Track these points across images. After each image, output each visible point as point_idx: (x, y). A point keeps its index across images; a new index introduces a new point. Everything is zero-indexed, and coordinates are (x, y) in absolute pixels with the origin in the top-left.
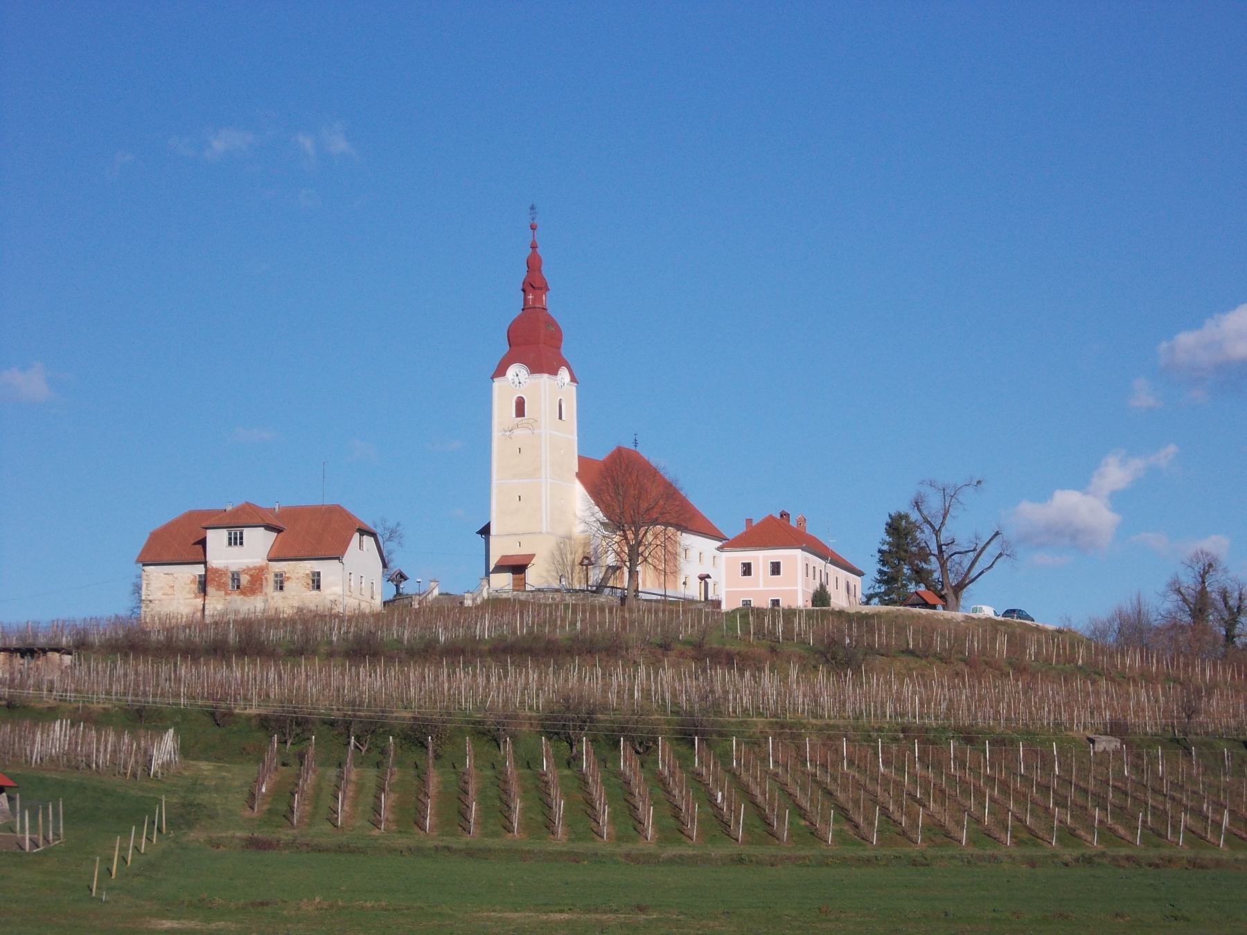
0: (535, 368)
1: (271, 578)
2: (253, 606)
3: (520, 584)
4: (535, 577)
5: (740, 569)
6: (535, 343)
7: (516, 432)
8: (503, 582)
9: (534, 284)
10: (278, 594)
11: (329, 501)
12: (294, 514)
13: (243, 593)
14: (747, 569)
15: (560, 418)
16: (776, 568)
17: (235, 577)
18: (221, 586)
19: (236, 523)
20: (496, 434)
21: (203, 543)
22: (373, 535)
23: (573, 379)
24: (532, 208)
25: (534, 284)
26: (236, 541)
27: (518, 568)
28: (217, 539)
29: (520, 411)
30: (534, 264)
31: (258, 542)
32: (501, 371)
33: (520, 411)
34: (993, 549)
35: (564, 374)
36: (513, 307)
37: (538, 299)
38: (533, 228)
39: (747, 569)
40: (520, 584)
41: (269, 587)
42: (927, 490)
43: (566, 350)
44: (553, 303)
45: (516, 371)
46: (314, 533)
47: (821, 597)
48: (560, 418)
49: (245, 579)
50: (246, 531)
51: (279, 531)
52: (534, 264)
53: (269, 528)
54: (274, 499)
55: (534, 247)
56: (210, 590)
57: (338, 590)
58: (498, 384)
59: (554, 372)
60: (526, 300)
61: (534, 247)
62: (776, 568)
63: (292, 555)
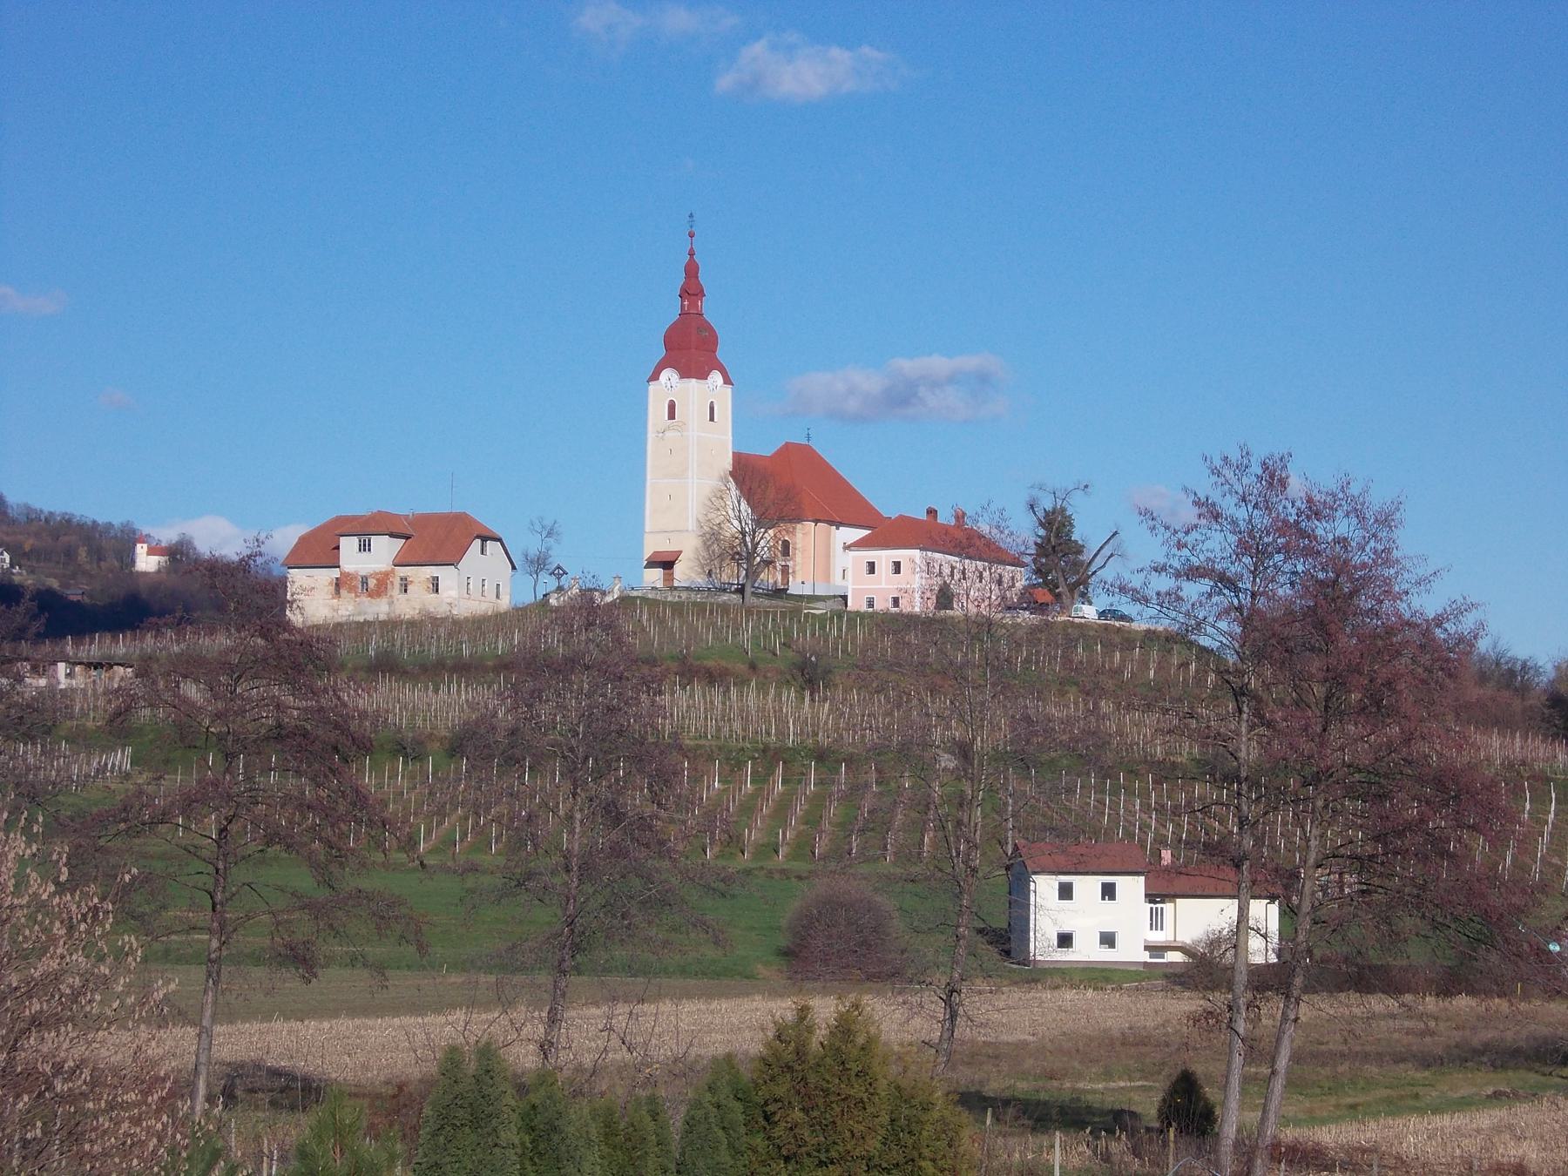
0: (685, 374)
1: (397, 582)
2: (378, 609)
3: (669, 578)
4: (684, 573)
5: (865, 567)
6: (691, 349)
7: (669, 434)
8: (655, 576)
9: (691, 291)
10: (403, 597)
11: (457, 509)
12: (424, 521)
13: (370, 596)
14: (871, 568)
15: (712, 419)
16: (897, 567)
17: (365, 581)
18: (352, 589)
19: (365, 529)
20: (651, 435)
21: (338, 548)
22: (499, 540)
23: (727, 381)
24: (691, 216)
25: (691, 291)
26: (365, 547)
27: (666, 563)
28: (348, 545)
29: (672, 416)
30: (692, 270)
31: (385, 549)
32: (655, 376)
33: (672, 416)
34: (1106, 552)
35: (716, 377)
36: (670, 310)
37: (693, 305)
38: (691, 235)
39: (871, 568)
40: (669, 578)
41: (395, 591)
42: (1035, 492)
43: (720, 354)
44: (711, 309)
45: (668, 375)
46: (439, 539)
47: (945, 597)
48: (712, 419)
49: (372, 583)
50: (373, 538)
51: (407, 538)
52: (692, 270)
53: (392, 535)
54: (404, 505)
55: (692, 254)
56: (343, 592)
57: (454, 593)
58: (653, 386)
59: (703, 375)
60: (682, 306)
61: (692, 254)
62: (897, 567)
63: (414, 561)
